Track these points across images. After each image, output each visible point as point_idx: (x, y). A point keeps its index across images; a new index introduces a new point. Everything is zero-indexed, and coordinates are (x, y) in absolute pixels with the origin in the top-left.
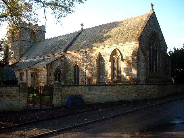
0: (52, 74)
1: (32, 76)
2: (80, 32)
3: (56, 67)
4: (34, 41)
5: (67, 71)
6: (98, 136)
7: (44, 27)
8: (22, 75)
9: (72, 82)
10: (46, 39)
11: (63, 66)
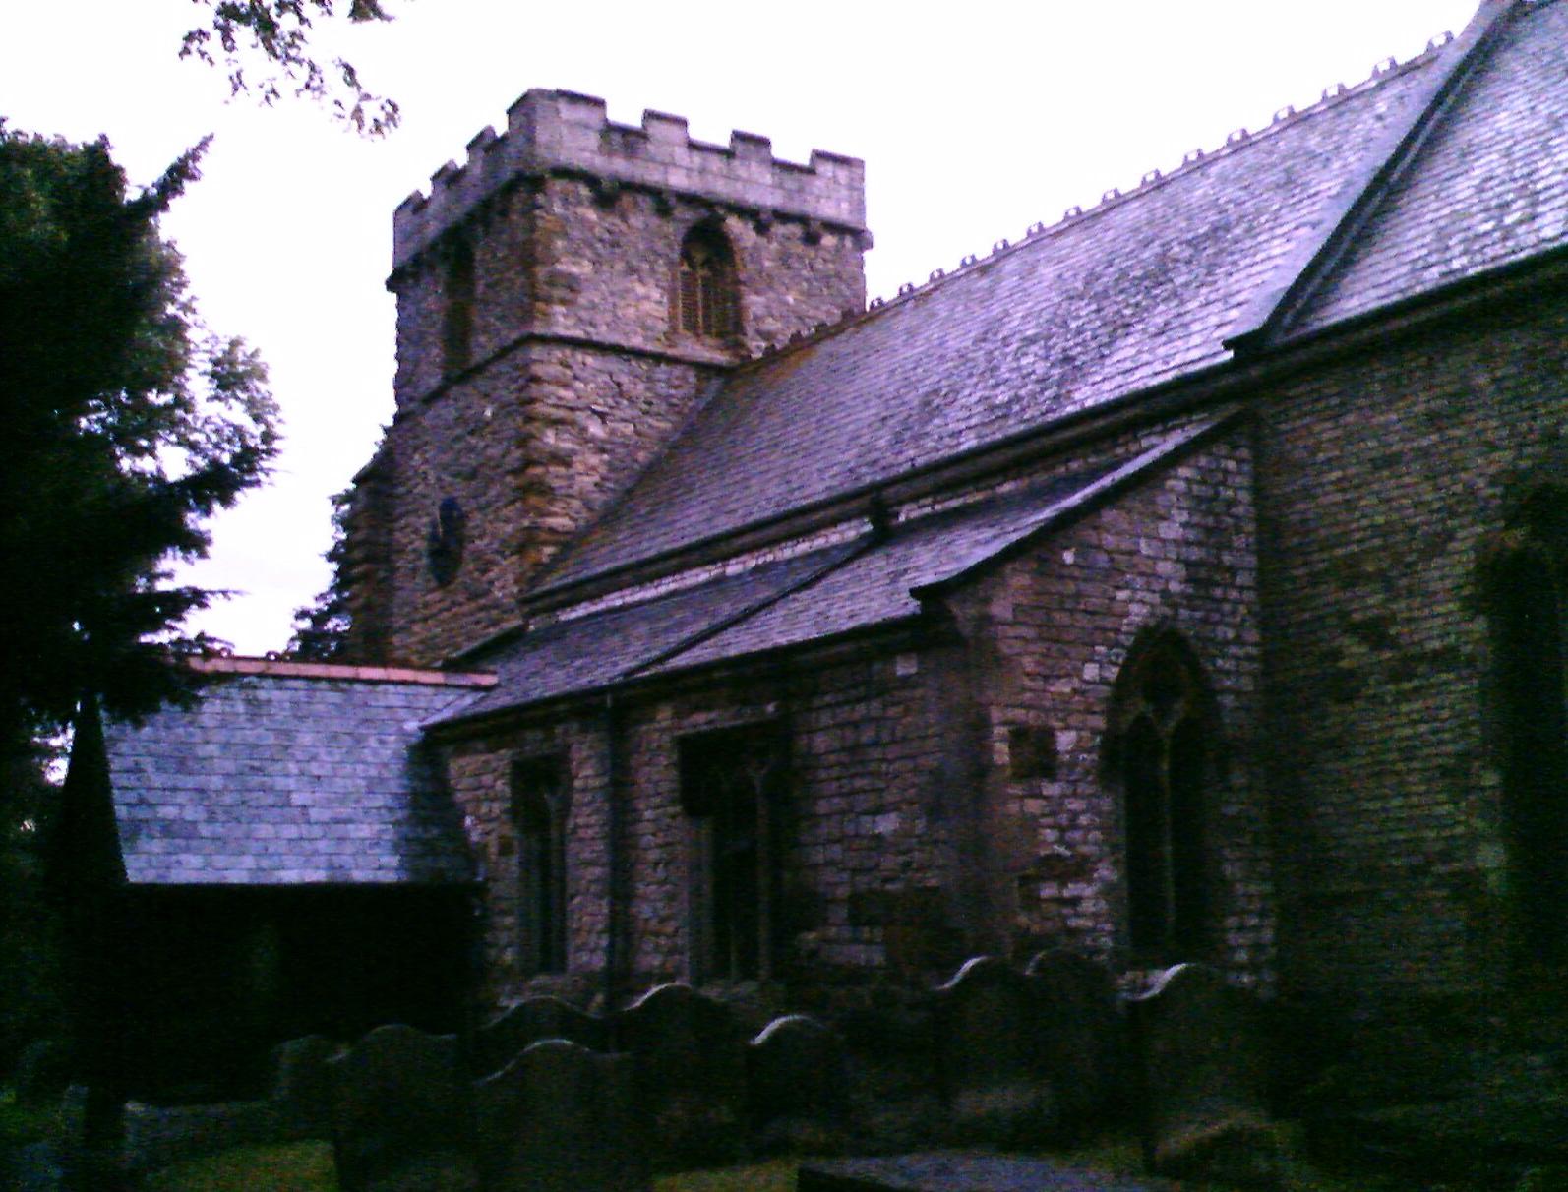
0: (1065, 740)
1: (694, 798)
2: (1453, 57)
3: (1137, 609)
4: (722, 358)
5: (1345, 687)
6: (288, 689)
7: (843, 174)
8: (553, 803)
9: (1466, 886)
10: (871, 297)
11: (1240, 595)
